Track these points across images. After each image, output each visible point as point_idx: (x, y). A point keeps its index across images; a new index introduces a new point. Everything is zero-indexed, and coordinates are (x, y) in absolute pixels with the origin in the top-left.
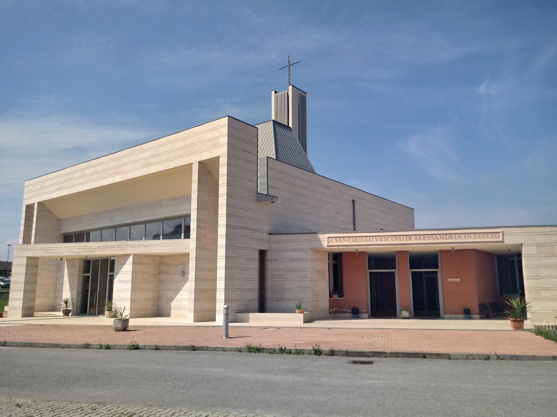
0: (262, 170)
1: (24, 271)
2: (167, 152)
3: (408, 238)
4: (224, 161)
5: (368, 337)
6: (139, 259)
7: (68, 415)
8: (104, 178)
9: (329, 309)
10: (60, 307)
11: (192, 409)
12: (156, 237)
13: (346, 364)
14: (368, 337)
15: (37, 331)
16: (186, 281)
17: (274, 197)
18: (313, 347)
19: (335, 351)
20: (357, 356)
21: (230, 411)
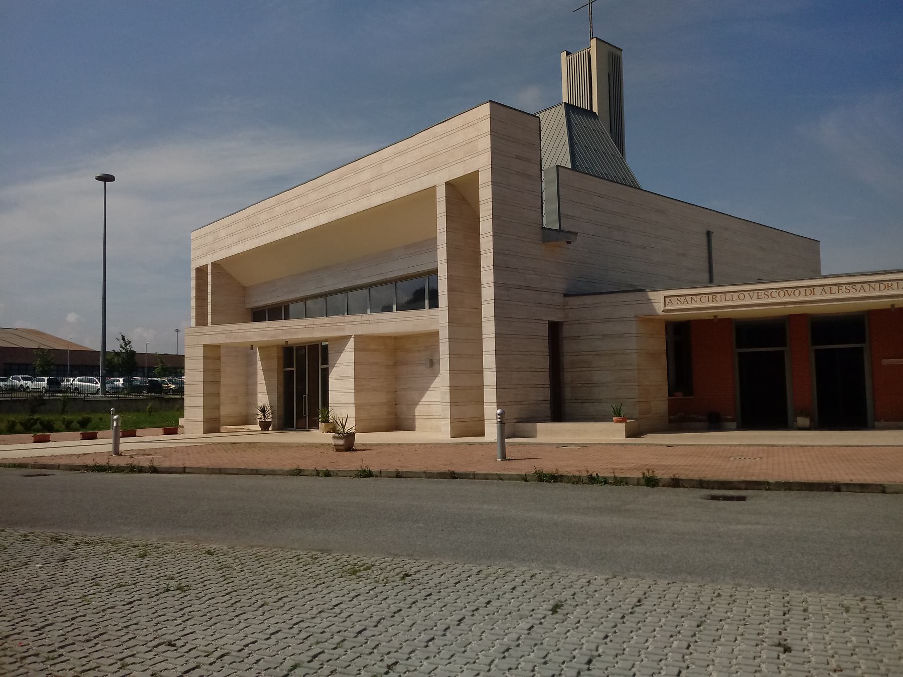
0: (549, 190)
1: (201, 366)
2: (394, 171)
3: (808, 292)
4: (485, 178)
5: (738, 458)
6: (364, 343)
7: (280, 566)
8: (303, 219)
9: (669, 416)
10: (254, 418)
11: (457, 561)
12: (387, 309)
13: (700, 500)
14: (738, 458)
15: (226, 451)
16: (435, 374)
17: (571, 233)
18: (644, 474)
19: (680, 479)
20: (719, 489)
21: (515, 565)
